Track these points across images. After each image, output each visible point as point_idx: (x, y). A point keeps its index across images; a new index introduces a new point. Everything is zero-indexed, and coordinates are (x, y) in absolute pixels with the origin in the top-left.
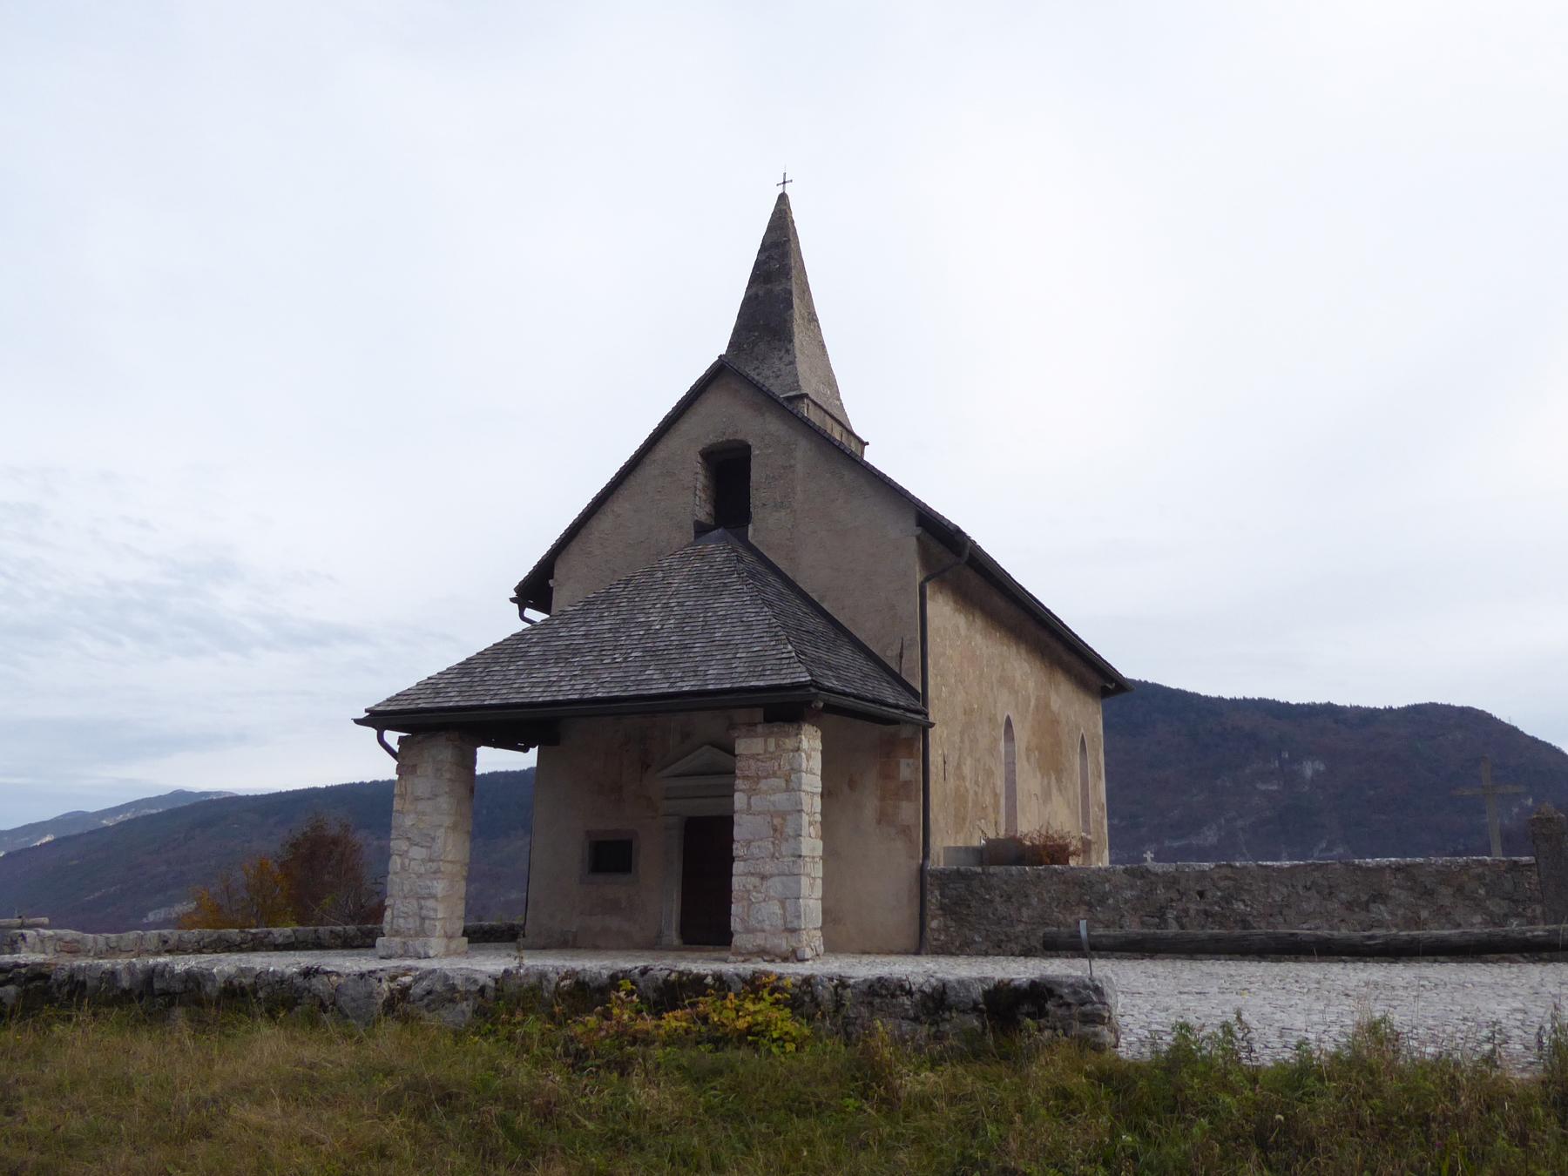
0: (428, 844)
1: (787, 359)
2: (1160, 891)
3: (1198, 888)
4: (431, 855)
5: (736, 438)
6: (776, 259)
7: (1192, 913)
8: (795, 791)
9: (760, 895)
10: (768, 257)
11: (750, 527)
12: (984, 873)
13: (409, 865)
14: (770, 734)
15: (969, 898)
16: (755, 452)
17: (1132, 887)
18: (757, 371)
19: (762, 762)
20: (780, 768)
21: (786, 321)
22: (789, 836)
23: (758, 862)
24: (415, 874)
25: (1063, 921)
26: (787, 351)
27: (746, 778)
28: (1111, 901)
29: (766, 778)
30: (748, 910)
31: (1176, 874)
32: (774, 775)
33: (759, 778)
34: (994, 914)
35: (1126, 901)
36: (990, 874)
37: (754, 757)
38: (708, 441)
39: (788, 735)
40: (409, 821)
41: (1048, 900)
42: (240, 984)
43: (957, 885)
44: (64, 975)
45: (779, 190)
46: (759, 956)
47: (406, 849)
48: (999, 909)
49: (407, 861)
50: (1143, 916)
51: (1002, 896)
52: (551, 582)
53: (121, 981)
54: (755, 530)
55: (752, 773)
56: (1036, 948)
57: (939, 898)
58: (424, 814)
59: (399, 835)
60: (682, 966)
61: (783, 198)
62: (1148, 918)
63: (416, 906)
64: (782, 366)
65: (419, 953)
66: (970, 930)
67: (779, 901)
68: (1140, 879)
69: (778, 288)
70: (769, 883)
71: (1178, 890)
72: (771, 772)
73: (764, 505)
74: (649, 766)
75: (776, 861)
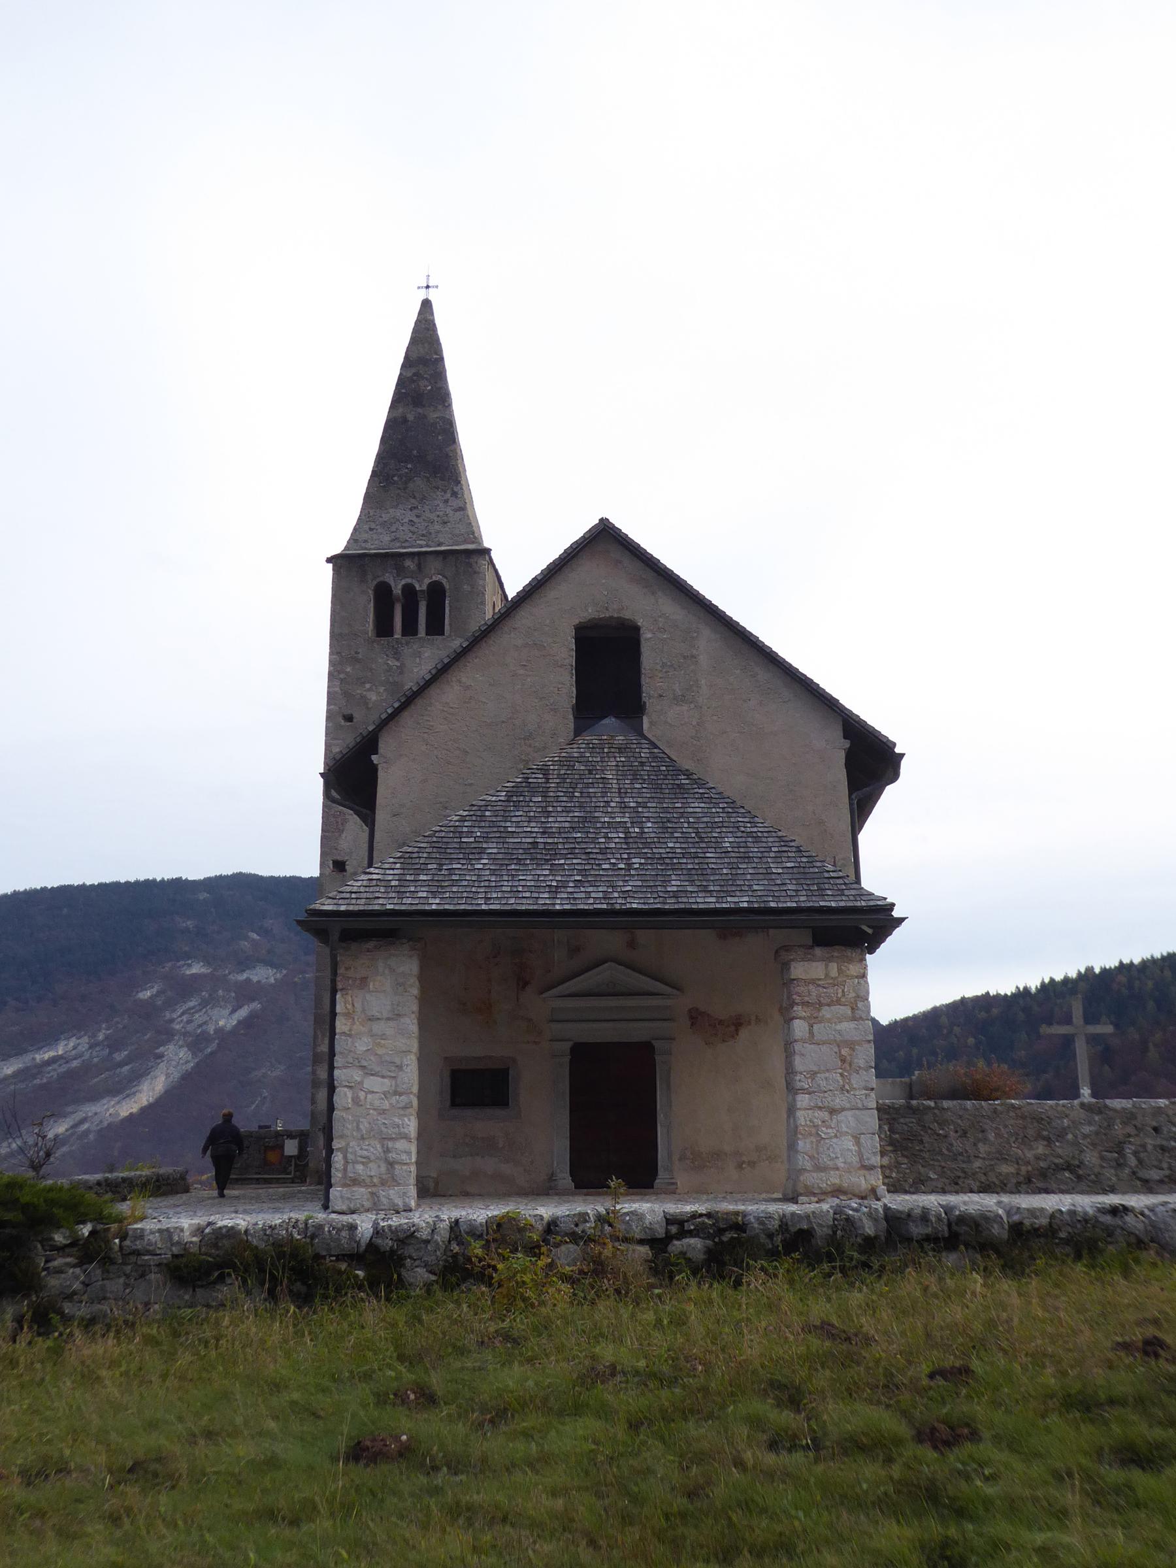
0: (393, 1075)
1: (455, 503)
2: (1118, 1127)
3: (1154, 1124)
4: (397, 1086)
5: (621, 615)
6: (427, 379)
7: (1150, 1147)
8: (863, 1020)
9: (829, 1131)
10: (414, 374)
11: (645, 720)
12: (937, 1107)
13: (366, 1098)
14: (830, 959)
15: (922, 1133)
16: (646, 635)
17: (1090, 1124)
18: (415, 511)
19: (824, 988)
20: (844, 995)
21: (447, 456)
22: (860, 1067)
23: (826, 1095)
24: (374, 1109)
25: (1023, 1157)
26: (455, 494)
27: (805, 1004)
28: (1070, 1136)
29: (829, 1005)
30: (817, 1145)
31: (1134, 1110)
32: (839, 1002)
33: (821, 1005)
34: (948, 1150)
35: (1085, 1136)
36: (943, 1109)
37: (813, 982)
38: (585, 614)
39: (850, 961)
40: (362, 1046)
41: (1006, 1136)
42: (1031, 1225)
43: (907, 1120)
44: (774, 1225)
45: (422, 295)
46: (833, 1196)
47: (358, 1079)
48: (955, 1144)
49: (362, 1095)
50: (1102, 1151)
51: (956, 1132)
52: (374, 758)
53: (864, 1228)
54: (651, 723)
55: (813, 999)
56: (995, 1184)
57: (888, 1133)
58: (383, 1036)
59: (348, 1063)
60: (225, 1221)
61: (426, 305)
62: (1105, 1153)
63: (380, 1150)
64: (449, 510)
65: (394, 1205)
66: (923, 1166)
67: (853, 1136)
68: (1097, 1114)
69: (433, 416)
70: (840, 1117)
71: (1135, 1126)
72: (835, 999)
73: (661, 696)
74: (526, 983)
75: (846, 1094)
